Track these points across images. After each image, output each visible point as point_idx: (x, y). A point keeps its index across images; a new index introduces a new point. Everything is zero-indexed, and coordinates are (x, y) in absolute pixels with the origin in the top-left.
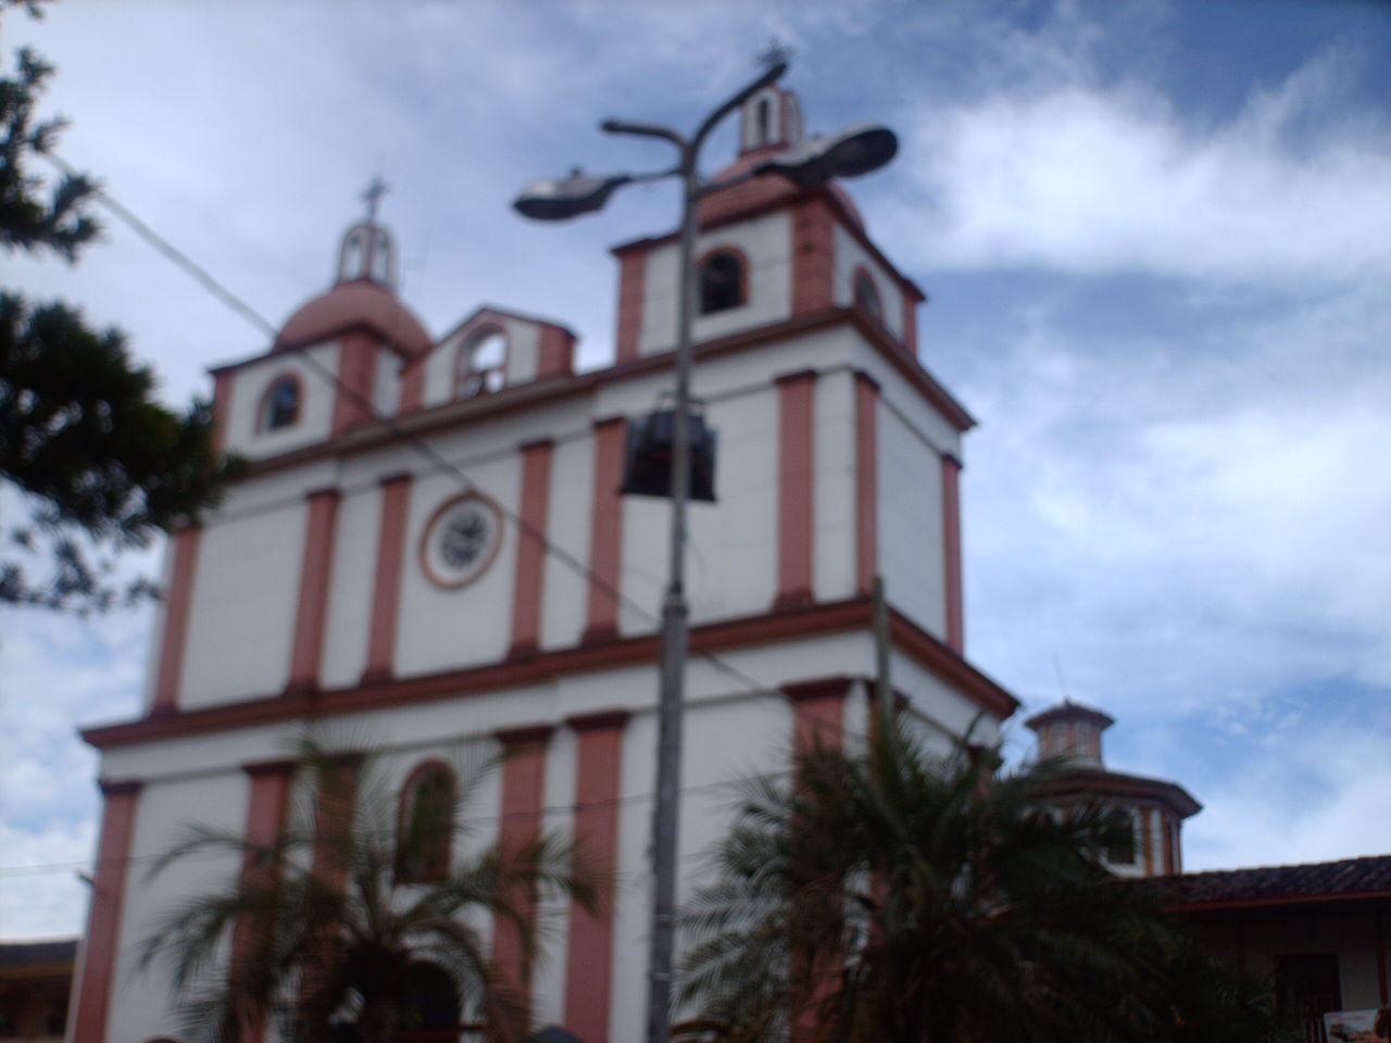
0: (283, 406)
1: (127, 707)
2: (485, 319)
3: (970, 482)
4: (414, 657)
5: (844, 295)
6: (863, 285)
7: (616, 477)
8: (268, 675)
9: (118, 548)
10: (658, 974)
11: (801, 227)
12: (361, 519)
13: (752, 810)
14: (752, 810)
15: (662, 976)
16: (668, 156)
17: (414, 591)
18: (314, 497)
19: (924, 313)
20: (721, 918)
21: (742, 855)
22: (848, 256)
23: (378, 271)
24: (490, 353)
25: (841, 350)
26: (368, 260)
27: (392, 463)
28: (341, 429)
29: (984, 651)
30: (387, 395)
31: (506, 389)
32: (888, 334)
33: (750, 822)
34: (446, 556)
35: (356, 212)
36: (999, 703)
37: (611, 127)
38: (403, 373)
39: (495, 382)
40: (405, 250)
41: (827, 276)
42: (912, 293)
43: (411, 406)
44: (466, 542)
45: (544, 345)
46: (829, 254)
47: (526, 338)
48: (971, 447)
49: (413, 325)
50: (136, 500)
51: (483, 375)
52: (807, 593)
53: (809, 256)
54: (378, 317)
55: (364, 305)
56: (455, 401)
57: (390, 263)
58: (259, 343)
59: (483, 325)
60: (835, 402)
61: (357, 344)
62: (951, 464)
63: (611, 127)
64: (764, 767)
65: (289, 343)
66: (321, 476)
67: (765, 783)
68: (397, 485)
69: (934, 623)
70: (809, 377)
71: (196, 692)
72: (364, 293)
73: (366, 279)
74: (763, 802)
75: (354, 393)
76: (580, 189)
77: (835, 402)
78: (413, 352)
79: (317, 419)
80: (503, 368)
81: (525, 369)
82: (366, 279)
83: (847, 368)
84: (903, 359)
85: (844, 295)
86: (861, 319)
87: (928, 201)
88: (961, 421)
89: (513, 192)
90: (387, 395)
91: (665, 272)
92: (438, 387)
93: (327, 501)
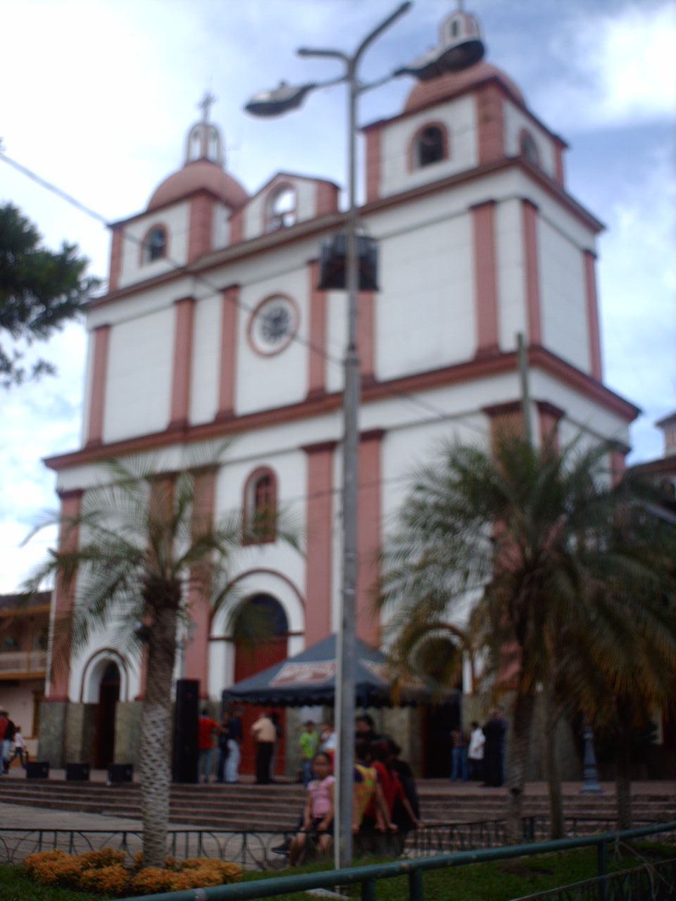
0: (156, 246)
1: (71, 438)
2: (281, 180)
3: (603, 268)
4: (247, 403)
5: (512, 148)
6: (526, 142)
7: (318, 279)
8: (157, 418)
9: (30, 341)
10: (348, 590)
11: (482, 105)
12: (210, 314)
13: (420, 488)
14: (420, 488)
15: (350, 592)
16: (337, 68)
17: (245, 358)
18: (179, 302)
19: (569, 157)
20: (405, 554)
21: (417, 516)
22: (514, 122)
23: (212, 153)
24: (285, 202)
25: (512, 185)
26: (205, 148)
27: (223, 279)
28: (194, 257)
29: (617, 379)
30: (222, 234)
31: (296, 225)
32: (545, 176)
33: (419, 496)
34: (265, 334)
35: (195, 116)
36: (629, 412)
37: (304, 52)
38: (230, 219)
39: (289, 221)
40: (229, 138)
41: (500, 136)
42: (560, 144)
43: (237, 241)
44: (277, 326)
45: (319, 194)
46: (502, 122)
47: (307, 191)
48: (603, 244)
49: (237, 186)
50: (37, 312)
51: (281, 216)
52: (496, 346)
53: (488, 123)
54: (213, 184)
55: (204, 176)
56: (263, 236)
57: (220, 148)
58: (140, 205)
59: (279, 184)
60: (509, 219)
61: (201, 202)
62: (590, 256)
63: (304, 52)
64: (426, 460)
65: (159, 205)
66: (183, 289)
67: (429, 473)
68: (230, 292)
69: (581, 361)
70: (491, 204)
71: (114, 431)
72: (203, 168)
73: (204, 159)
74: (426, 482)
75: (201, 230)
76: (285, 95)
77: (509, 219)
78: (236, 204)
79: (178, 252)
80: (293, 211)
81: (308, 211)
82: (204, 159)
83: (516, 197)
84: (555, 189)
85: (512, 148)
86: (525, 163)
87: (587, 82)
88: (594, 226)
89: (244, 99)
90: (222, 234)
91: (398, 142)
92: (253, 226)
93: (189, 302)
